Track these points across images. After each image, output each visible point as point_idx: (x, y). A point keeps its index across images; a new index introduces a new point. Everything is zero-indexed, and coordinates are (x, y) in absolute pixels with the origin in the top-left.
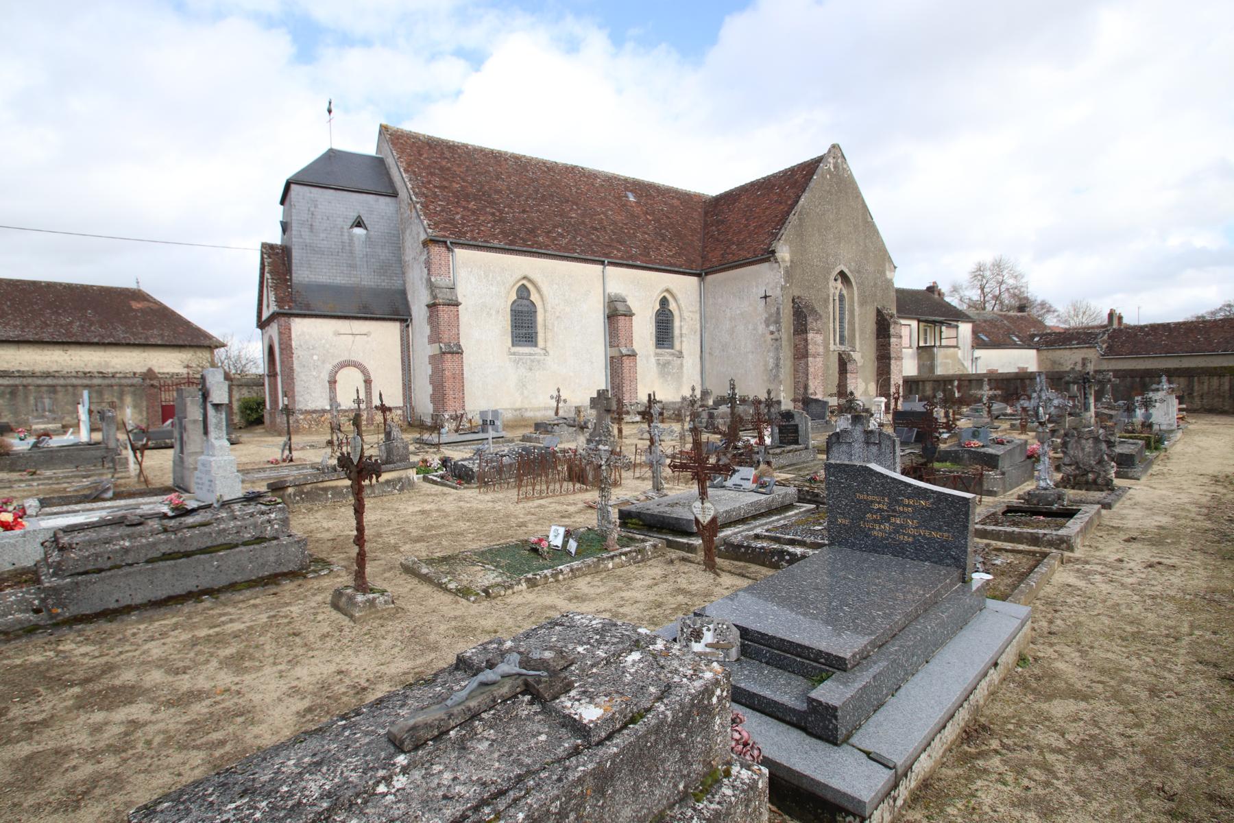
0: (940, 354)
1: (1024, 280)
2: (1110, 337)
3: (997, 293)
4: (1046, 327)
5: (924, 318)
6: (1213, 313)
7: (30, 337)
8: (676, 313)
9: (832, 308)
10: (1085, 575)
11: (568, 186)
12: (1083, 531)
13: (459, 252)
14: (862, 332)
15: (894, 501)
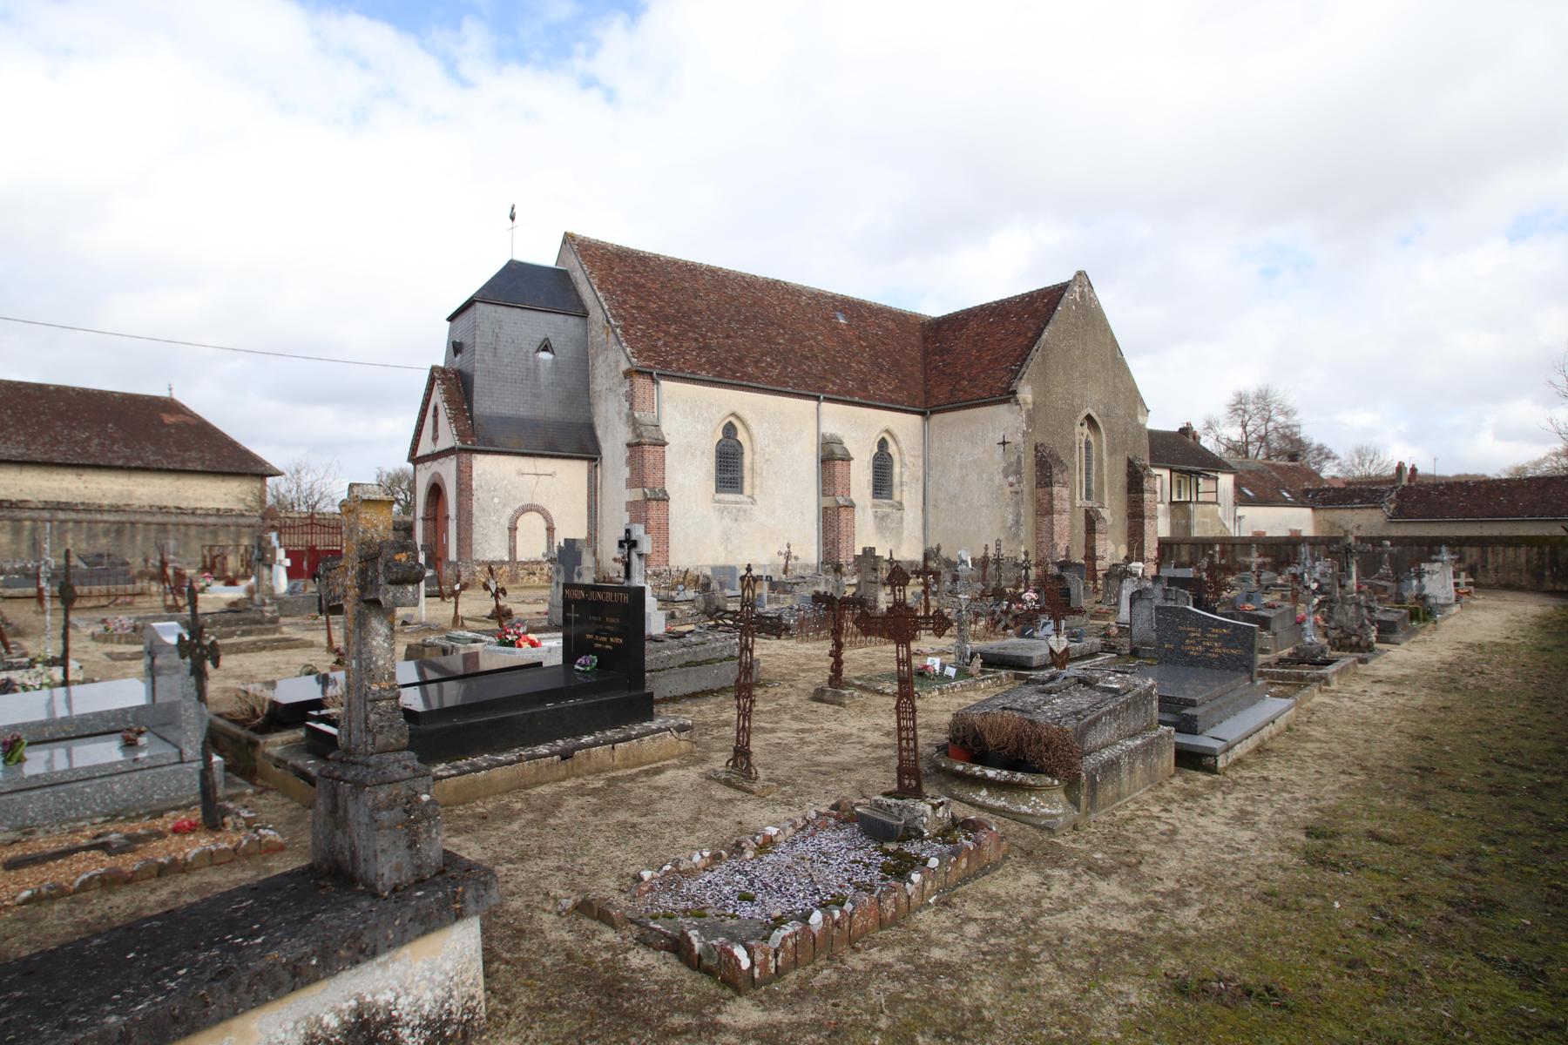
0: (1197, 512)
2: (1398, 496)
3: (1263, 432)
4: (1322, 480)
6: (1537, 464)
7: (38, 457)
8: (896, 457)
9: (1079, 458)
10: (1337, 699)
11: (771, 305)
12: (1340, 673)
13: (666, 385)
14: (1111, 485)
15: (1206, 630)
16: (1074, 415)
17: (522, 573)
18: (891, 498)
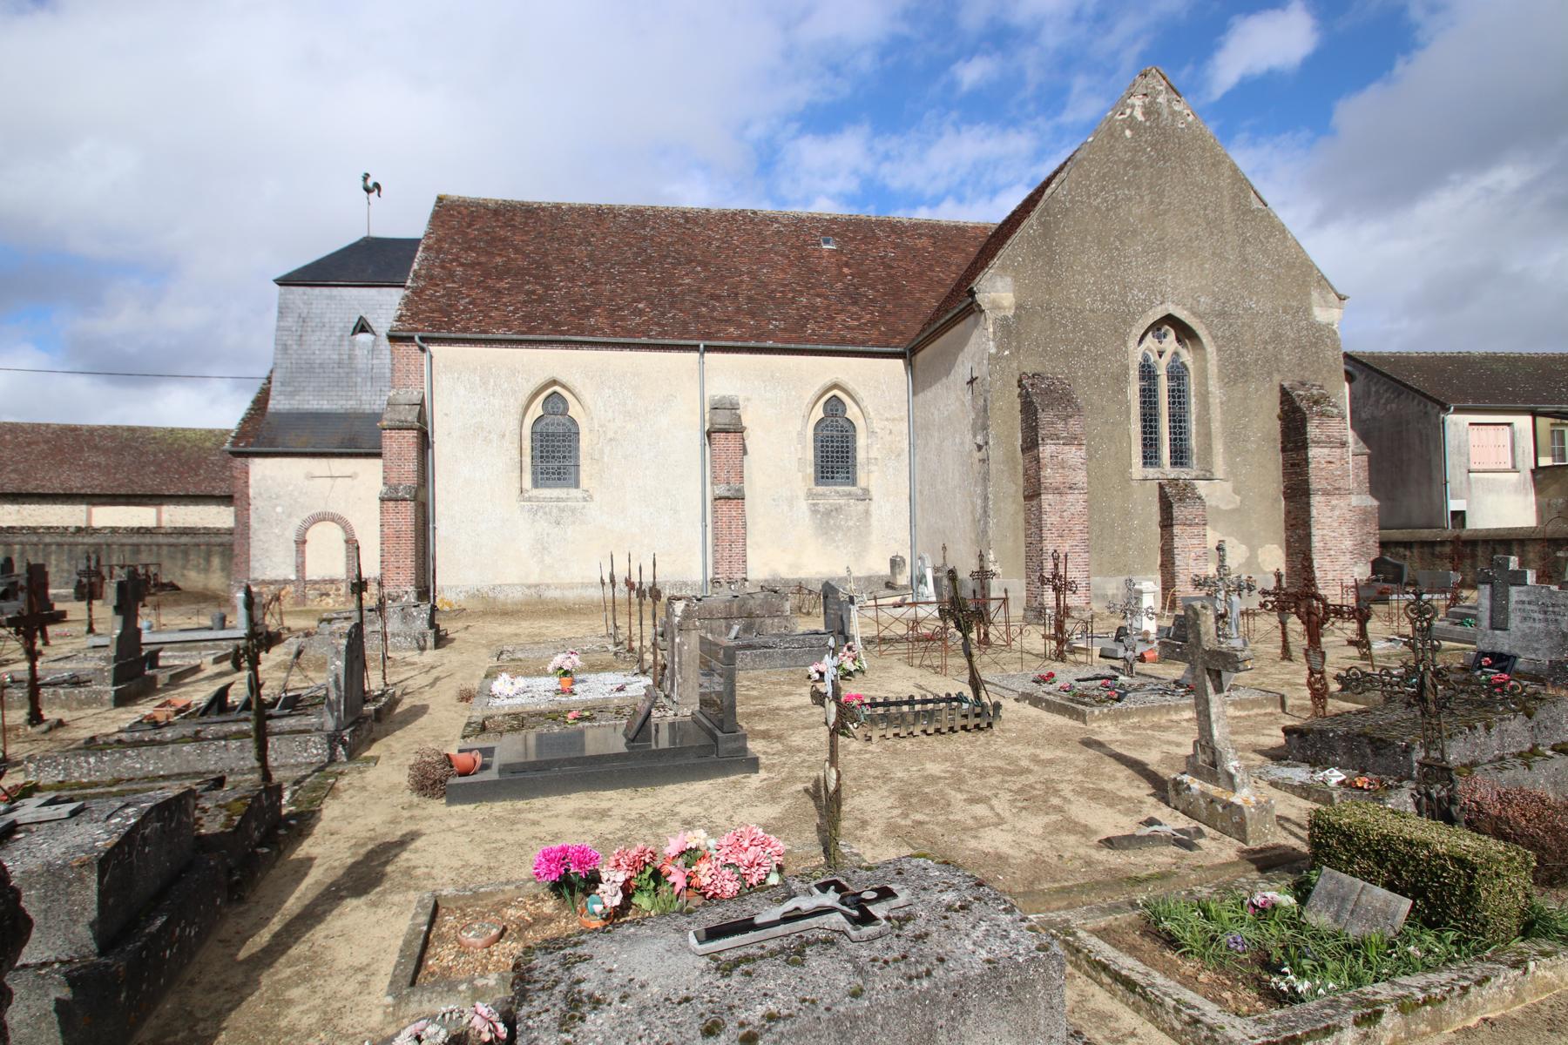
8: (860, 424)
14: (1234, 438)
16: (1128, 319)
17: (311, 593)
18: (577, 486)
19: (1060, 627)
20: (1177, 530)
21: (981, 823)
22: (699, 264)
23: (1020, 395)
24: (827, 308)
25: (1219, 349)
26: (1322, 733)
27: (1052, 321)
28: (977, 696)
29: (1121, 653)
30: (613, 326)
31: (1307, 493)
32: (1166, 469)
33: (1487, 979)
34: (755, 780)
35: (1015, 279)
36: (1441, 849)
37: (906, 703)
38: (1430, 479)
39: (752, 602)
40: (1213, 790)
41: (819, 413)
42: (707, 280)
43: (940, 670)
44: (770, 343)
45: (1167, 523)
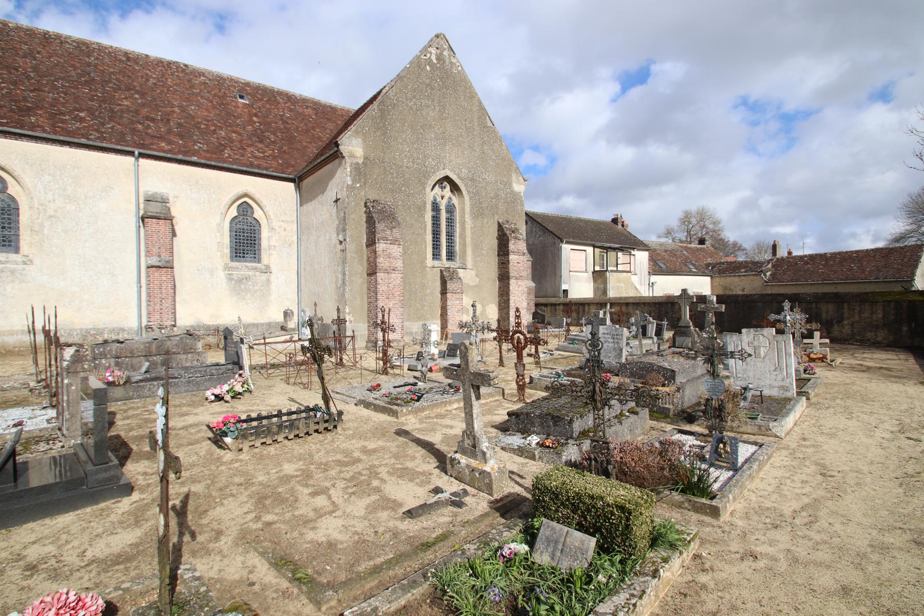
0: (612, 278)
1: (721, 225)
2: (773, 266)
5: (599, 244)
8: (263, 222)
14: (477, 247)
16: (426, 175)
19: (385, 353)
20: (449, 295)
21: (320, 514)
22: (137, 92)
23: (365, 212)
24: (241, 141)
25: (471, 199)
26: (528, 414)
27: (385, 169)
28: (328, 407)
29: (419, 368)
30: (53, 126)
31: (508, 278)
32: (444, 262)
33: (644, 592)
34: (125, 504)
35: (364, 141)
36: (610, 500)
37: (275, 416)
38: (555, 274)
39: (169, 343)
40: (473, 463)
41: (233, 212)
42: (143, 105)
43: (306, 386)
44: (195, 159)
45: (444, 292)
